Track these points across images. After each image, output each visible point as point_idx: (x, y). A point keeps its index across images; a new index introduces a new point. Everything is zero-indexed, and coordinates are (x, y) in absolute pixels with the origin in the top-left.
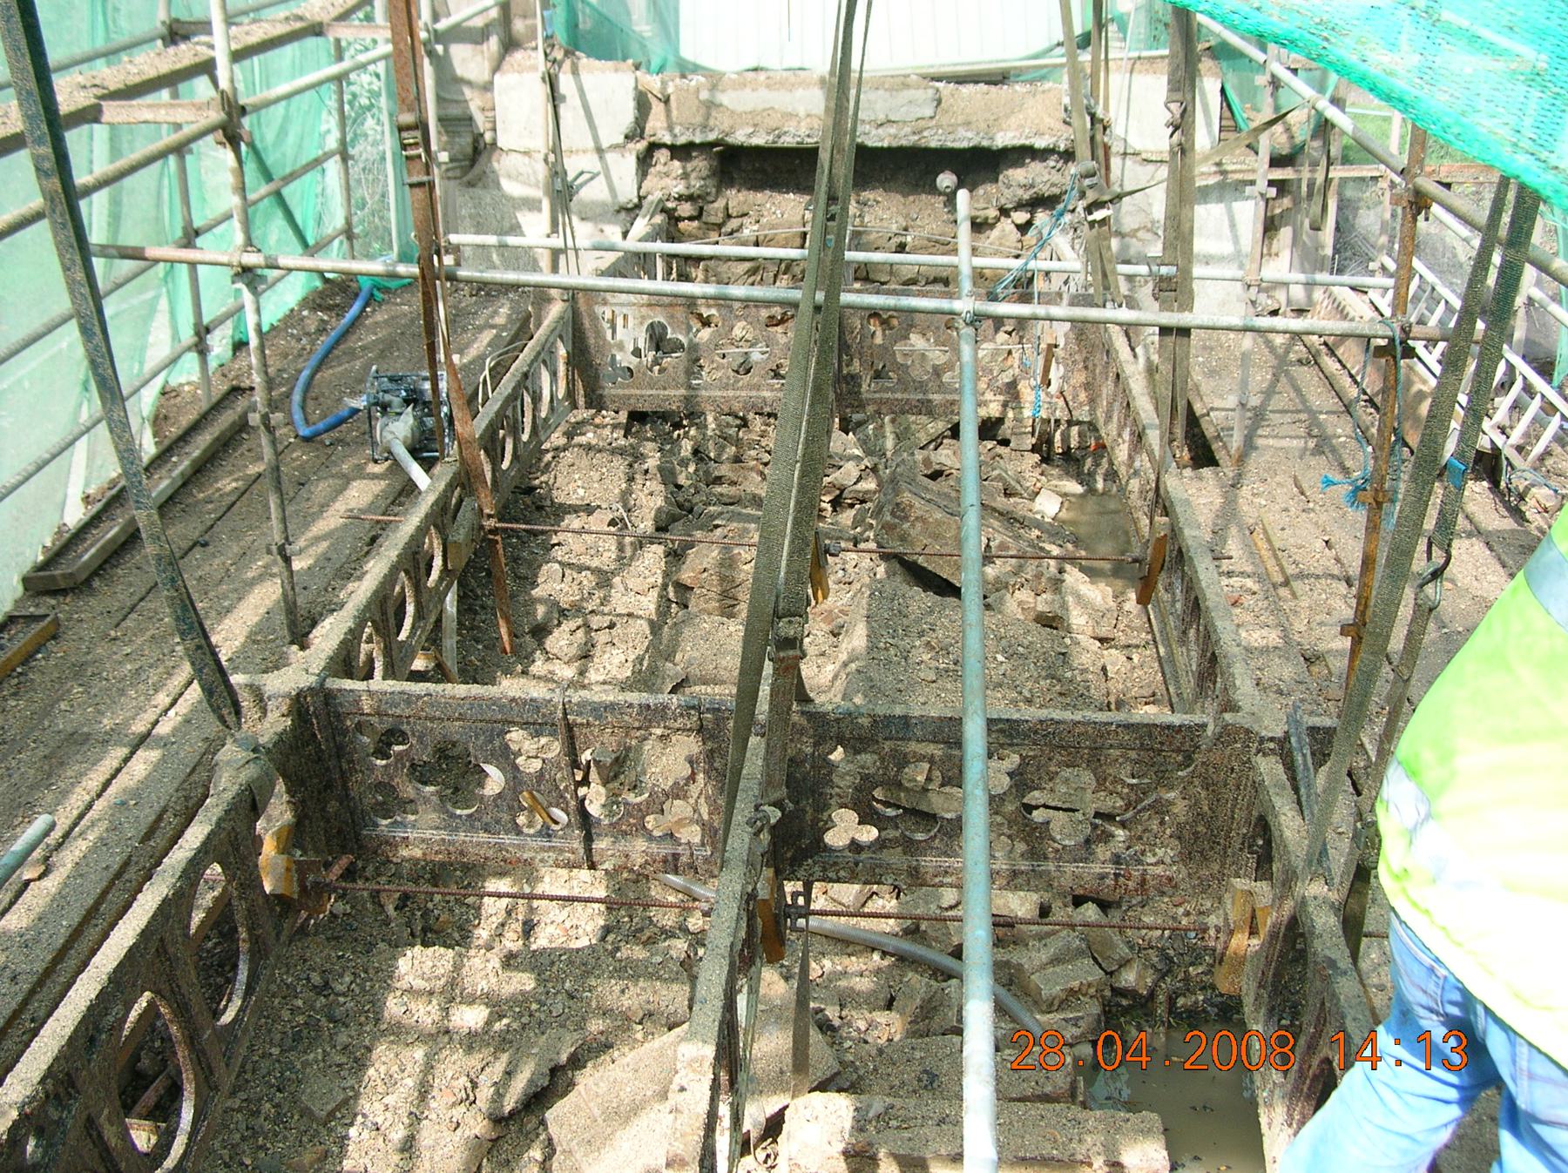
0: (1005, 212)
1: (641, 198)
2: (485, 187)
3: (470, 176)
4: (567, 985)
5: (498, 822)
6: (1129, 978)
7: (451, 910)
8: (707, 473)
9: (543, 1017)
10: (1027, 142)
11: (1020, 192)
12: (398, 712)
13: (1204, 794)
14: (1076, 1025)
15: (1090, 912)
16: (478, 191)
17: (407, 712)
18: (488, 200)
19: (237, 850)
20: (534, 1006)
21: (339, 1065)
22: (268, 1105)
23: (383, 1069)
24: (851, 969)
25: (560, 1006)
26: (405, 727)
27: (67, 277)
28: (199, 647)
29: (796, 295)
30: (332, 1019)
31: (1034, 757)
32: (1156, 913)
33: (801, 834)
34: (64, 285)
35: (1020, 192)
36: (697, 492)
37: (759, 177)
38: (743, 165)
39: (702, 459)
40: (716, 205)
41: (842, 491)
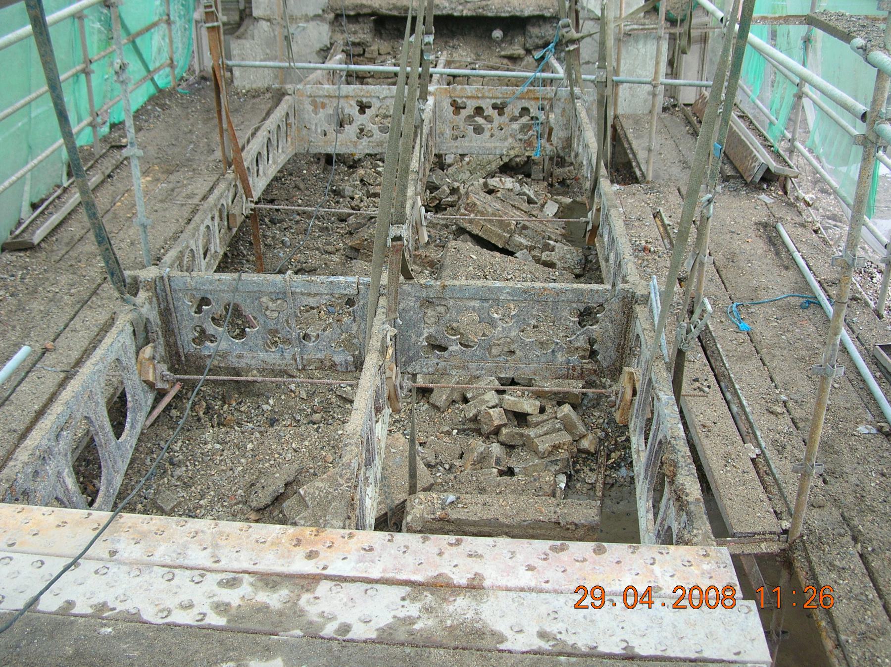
0: (528, 52)
1: (332, 44)
2: (245, 38)
3: (237, 33)
4: (294, 445)
5: (256, 345)
6: (585, 444)
7: (232, 414)
8: (368, 191)
9: (281, 460)
10: (541, 13)
11: (537, 41)
12: (206, 288)
13: (610, 325)
14: (557, 464)
15: (567, 409)
16: (243, 41)
17: (211, 288)
18: (248, 46)
19: (126, 354)
20: (277, 456)
21: (176, 486)
22: (140, 506)
23: (199, 487)
24: (492, 576)
25: (290, 456)
26: (209, 297)
27: (42, 59)
28: (107, 249)
29: (397, 69)
30: (172, 463)
31: (525, 307)
32: (601, 411)
33: (409, 349)
34: (41, 64)
35: (537, 41)
36: (362, 201)
37: (396, 32)
38: (387, 26)
39: (364, 185)
40: (372, 48)
41: (440, 202)
